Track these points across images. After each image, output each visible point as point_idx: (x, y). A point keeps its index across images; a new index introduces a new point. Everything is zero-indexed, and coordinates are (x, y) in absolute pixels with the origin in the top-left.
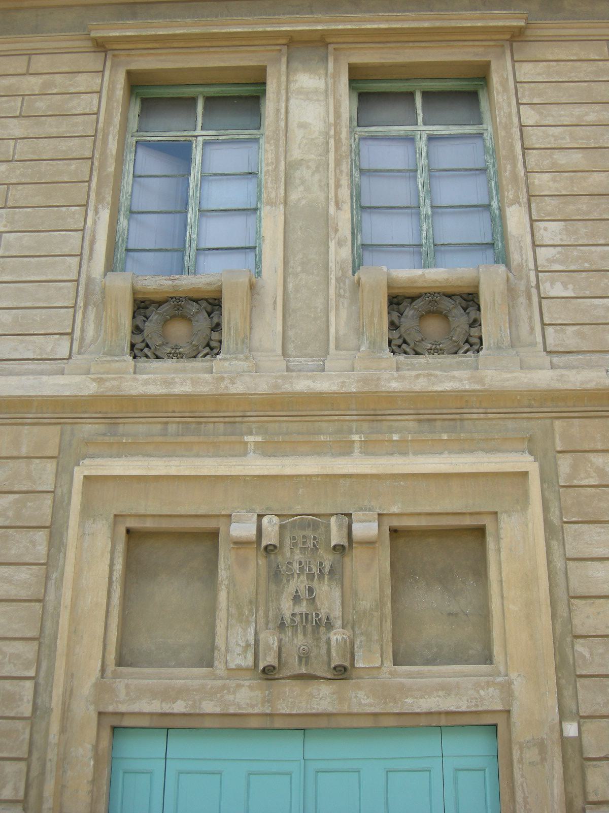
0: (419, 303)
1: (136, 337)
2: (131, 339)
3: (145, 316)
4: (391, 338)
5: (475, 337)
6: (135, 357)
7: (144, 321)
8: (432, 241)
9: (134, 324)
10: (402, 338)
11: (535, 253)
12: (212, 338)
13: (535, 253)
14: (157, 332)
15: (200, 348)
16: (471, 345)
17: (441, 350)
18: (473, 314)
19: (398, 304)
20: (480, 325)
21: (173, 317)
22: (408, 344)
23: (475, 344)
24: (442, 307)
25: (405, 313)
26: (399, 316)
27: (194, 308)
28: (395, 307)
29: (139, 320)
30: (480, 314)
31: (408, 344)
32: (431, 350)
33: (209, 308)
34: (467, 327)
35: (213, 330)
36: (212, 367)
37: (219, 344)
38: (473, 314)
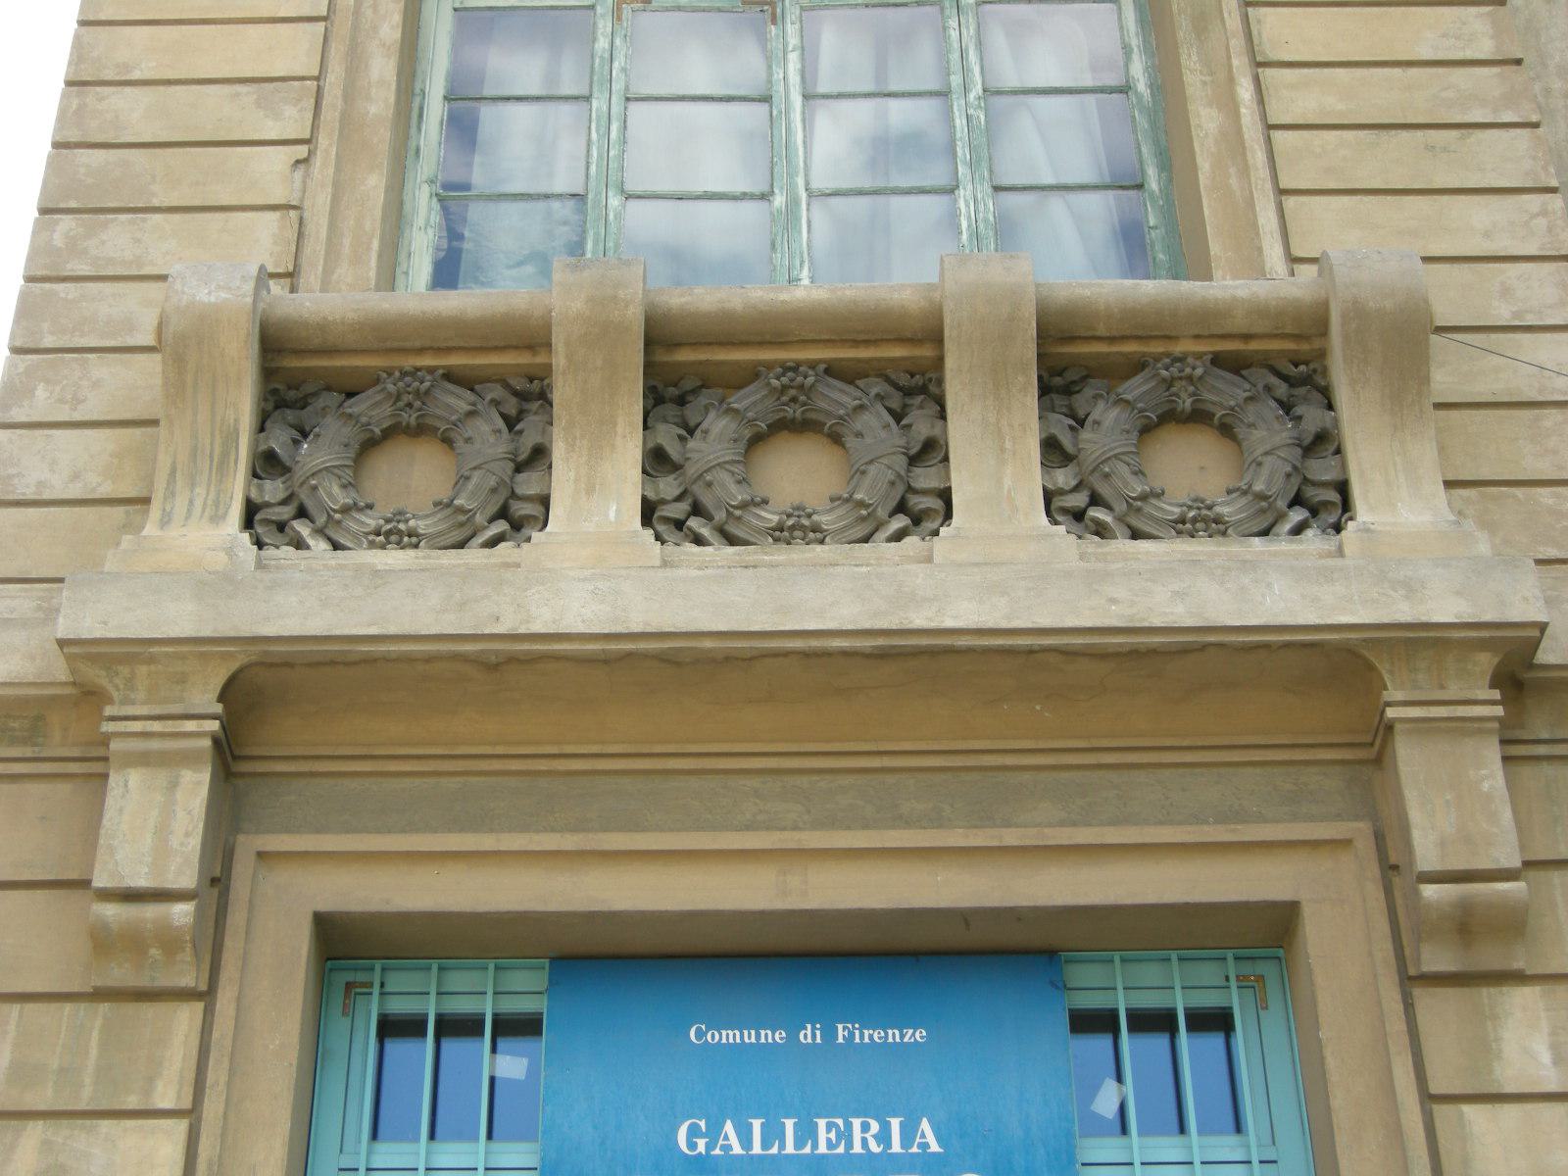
0: (1135, 388)
1: (268, 484)
2: (643, 489)
3: (1073, 417)
4: (651, 495)
5: (1324, 484)
6: (260, 544)
7: (682, 438)
8: (961, 81)
9: (651, 445)
10: (690, 500)
11: (1268, 141)
12: (519, 491)
13: (1268, 141)
14: (1126, 458)
15: (480, 519)
16: (1314, 512)
17: (814, 531)
18: (1313, 418)
19: (1068, 391)
20: (946, 459)
21: (1170, 417)
22: (709, 518)
23: (1326, 504)
24: (823, 404)
25: (1095, 415)
26: (1071, 428)
27: (457, 401)
28: (1059, 400)
29: (278, 440)
30: (945, 427)
31: (709, 518)
32: (782, 530)
33: (511, 406)
34: (901, 462)
35: (914, 460)
36: (931, 550)
37: (542, 509)
38: (922, 427)
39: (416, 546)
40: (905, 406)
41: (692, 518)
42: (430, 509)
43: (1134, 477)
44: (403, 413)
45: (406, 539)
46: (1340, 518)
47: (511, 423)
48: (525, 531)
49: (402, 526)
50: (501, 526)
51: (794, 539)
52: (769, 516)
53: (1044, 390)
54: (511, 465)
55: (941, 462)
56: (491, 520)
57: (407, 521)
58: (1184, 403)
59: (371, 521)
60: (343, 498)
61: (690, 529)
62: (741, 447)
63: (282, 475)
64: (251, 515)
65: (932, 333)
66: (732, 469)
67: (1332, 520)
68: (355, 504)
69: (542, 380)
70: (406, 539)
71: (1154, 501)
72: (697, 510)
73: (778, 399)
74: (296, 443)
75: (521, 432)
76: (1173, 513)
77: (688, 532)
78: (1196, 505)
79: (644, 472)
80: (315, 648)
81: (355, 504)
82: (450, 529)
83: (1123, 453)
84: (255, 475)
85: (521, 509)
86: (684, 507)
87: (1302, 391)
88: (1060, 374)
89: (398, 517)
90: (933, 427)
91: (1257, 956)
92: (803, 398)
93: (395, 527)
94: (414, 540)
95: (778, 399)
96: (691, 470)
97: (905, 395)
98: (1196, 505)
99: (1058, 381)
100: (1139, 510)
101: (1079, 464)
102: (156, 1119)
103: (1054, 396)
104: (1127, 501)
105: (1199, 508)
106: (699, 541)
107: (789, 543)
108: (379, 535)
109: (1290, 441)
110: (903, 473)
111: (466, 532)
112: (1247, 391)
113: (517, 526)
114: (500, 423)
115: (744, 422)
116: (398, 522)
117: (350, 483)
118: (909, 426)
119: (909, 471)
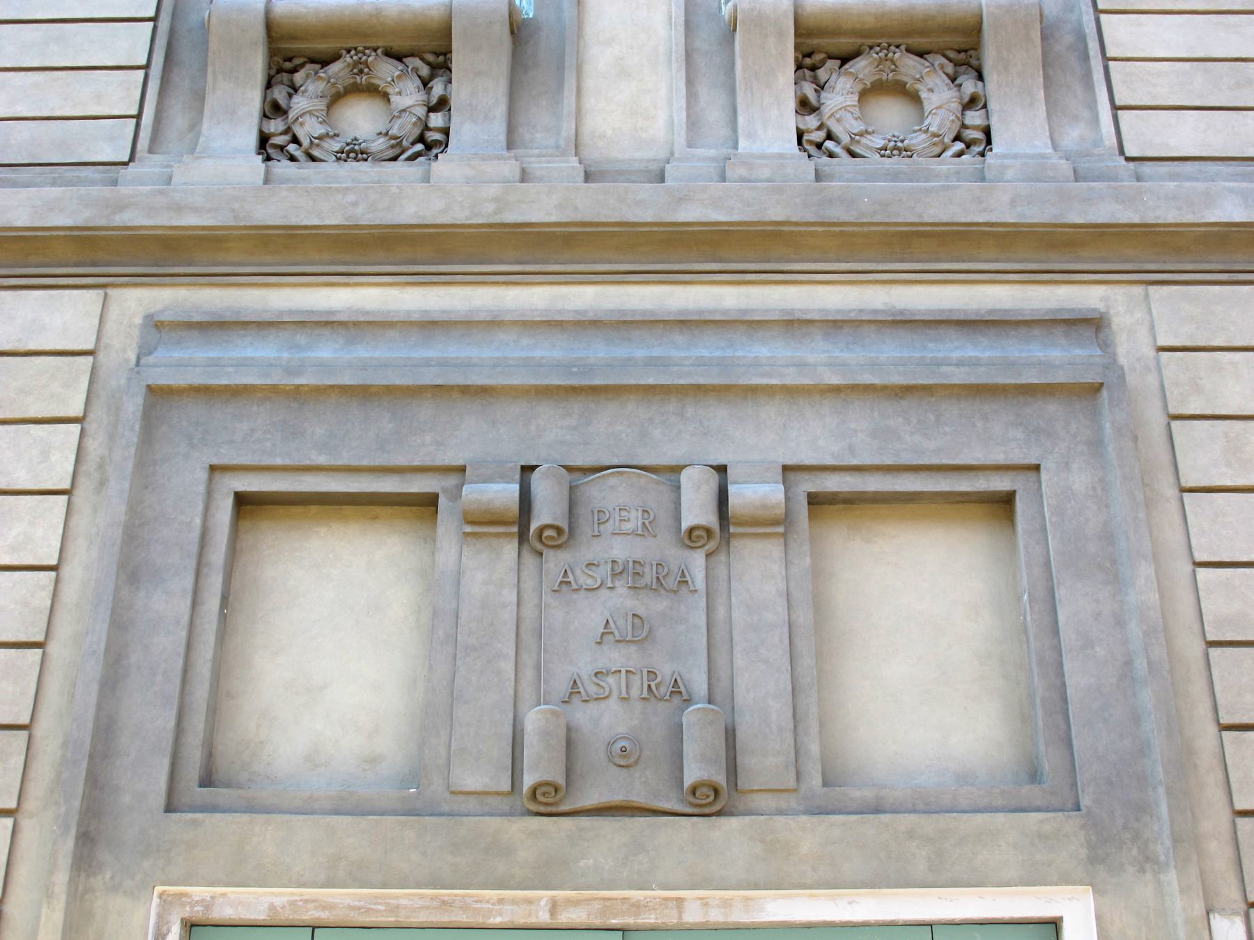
4: (802, 127)
6: (268, 158)
12: (967, 122)
17: (906, 151)
22: (838, 142)
26: (816, 90)
31: (838, 142)
35: (432, 109)
39: (366, 160)
40: (956, 72)
41: (827, 141)
42: (375, 137)
43: (319, 125)
44: (357, 76)
45: (360, 155)
46: (985, 149)
47: (425, 83)
48: (435, 151)
49: (356, 147)
50: (420, 147)
51: (349, 158)
52: (878, 141)
53: (799, 67)
54: (426, 108)
55: (982, 108)
56: (413, 144)
57: (360, 144)
58: (888, 75)
59: (336, 146)
60: (320, 130)
61: (288, 152)
62: (325, 101)
63: (282, 116)
64: (264, 141)
65: (446, 32)
66: (852, 110)
67: (981, 149)
68: (328, 134)
69: (445, 55)
70: (360, 155)
71: (869, 137)
72: (830, 136)
73: (352, 70)
74: (290, 96)
75: (432, 88)
76: (878, 144)
77: (287, 154)
78: (893, 139)
79: (796, 112)
80: (793, 229)
81: (328, 134)
82: (387, 149)
83: (316, 110)
84: (265, 116)
85: (433, 136)
86: (287, 138)
87: (964, 68)
88: (290, 60)
89: (354, 142)
90: (976, 85)
91: (951, 410)
92: (366, 70)
93: (353, 148)
94: (365, 156)
95: (352, 70)
96: (292, 115)
97: (955, 65)
98: (893, 139)
99: (808, 61)
100: (858, 142)
101: (820, 113)
102: (228, 540)
103: (284, 74)
104: (850, 136)
105: (896, 142)
106: (293, 159)
107: (346, 161)
108: (342, 152)
109: (422, 103)
110: (959, 115)
111: (397, 151)
112: (928, 67)
113: (429, 147)
114: (418, 82)
115: (857, 80)
116: (355, 145)
117: (324, 120)
118: (960, 85)
119: (963, 114)
